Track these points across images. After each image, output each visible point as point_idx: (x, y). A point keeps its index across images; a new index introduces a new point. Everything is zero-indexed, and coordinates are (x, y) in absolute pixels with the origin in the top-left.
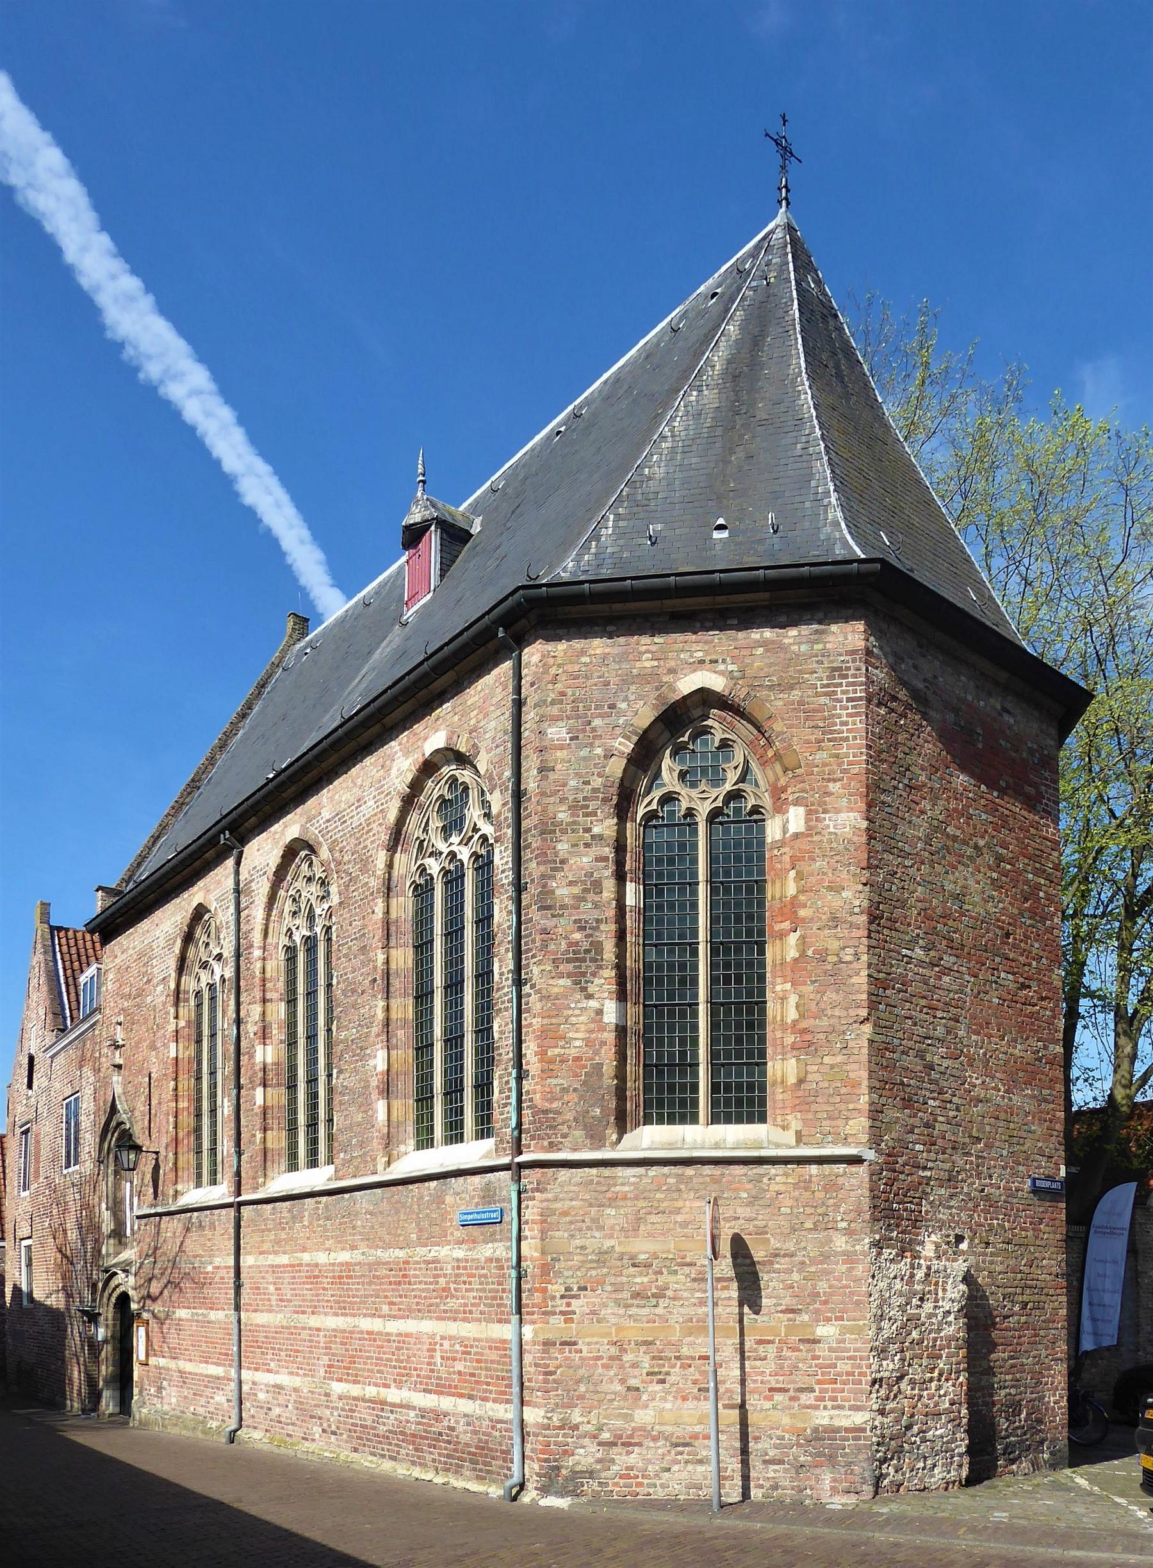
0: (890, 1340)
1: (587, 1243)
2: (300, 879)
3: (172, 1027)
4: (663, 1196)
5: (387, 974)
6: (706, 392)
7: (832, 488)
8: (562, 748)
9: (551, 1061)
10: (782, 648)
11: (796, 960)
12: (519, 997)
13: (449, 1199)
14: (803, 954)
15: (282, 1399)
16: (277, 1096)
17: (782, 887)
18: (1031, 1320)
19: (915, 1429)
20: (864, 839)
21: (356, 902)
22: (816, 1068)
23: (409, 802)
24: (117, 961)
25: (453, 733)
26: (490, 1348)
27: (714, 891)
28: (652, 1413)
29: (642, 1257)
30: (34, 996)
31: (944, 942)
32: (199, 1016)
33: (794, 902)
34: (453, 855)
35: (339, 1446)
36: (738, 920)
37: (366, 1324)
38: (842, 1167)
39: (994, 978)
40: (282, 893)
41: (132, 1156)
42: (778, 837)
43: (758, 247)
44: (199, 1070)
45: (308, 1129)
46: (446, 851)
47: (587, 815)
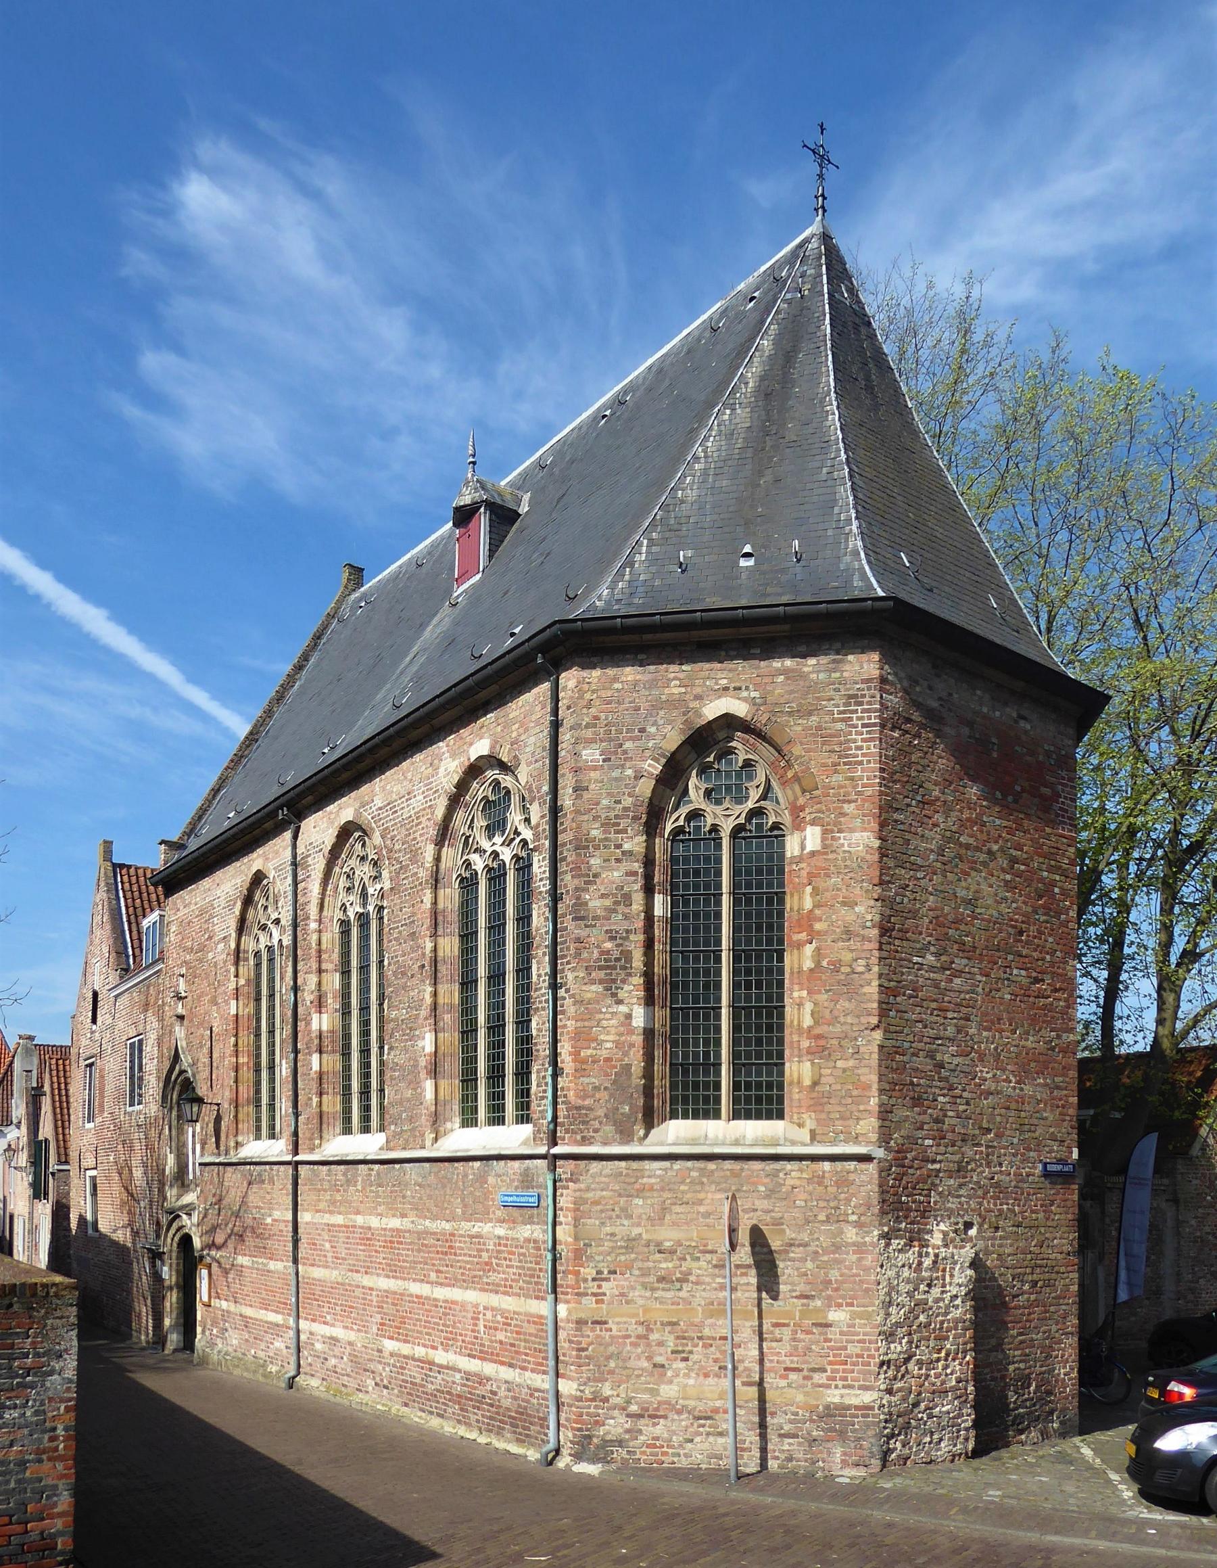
0: (898, 1325)
1: (617, 1230)
2: (354, 857)
3: (232, 986)
4: (686, 1188)
5: (435, 961)
6: (739, 411)
7: (854, 515)
8: (595, 768)
9: (584, 1061)
10: (803, 676)
11: (811, 970)
12: (555, 999)
13: (491, 1180)
14: (818, 964)
15: (337, 1351)
16: (333, 1062)
17: (800, 901)
18: (1041, 1297)
19: (923, 1406)
20: (876, 857)
21: (406, 890)
22: (829, 1071)
23: (455, 801)
24: (180, 914)
25: (497, 742)
26: (529, 1322)
27: (736, 902)
28: (676, 1388)
29: (668, 1244)
30: (98, 933)
31: (956, 946)
32: (258, 975)
33: (811, 917)
34: (495, 855)
35: (391, 1400)
36: (759, 928)
37: (416, 1288)
38: (852, 1165)
39: (1006, 976)
40: (337, 869)
41: (195, 1109)
42: (796, 853)
43: (794, 254)
44: (258, 1028)
45: (362, 1103)
46: (490, 850)
47: (617, 832)
